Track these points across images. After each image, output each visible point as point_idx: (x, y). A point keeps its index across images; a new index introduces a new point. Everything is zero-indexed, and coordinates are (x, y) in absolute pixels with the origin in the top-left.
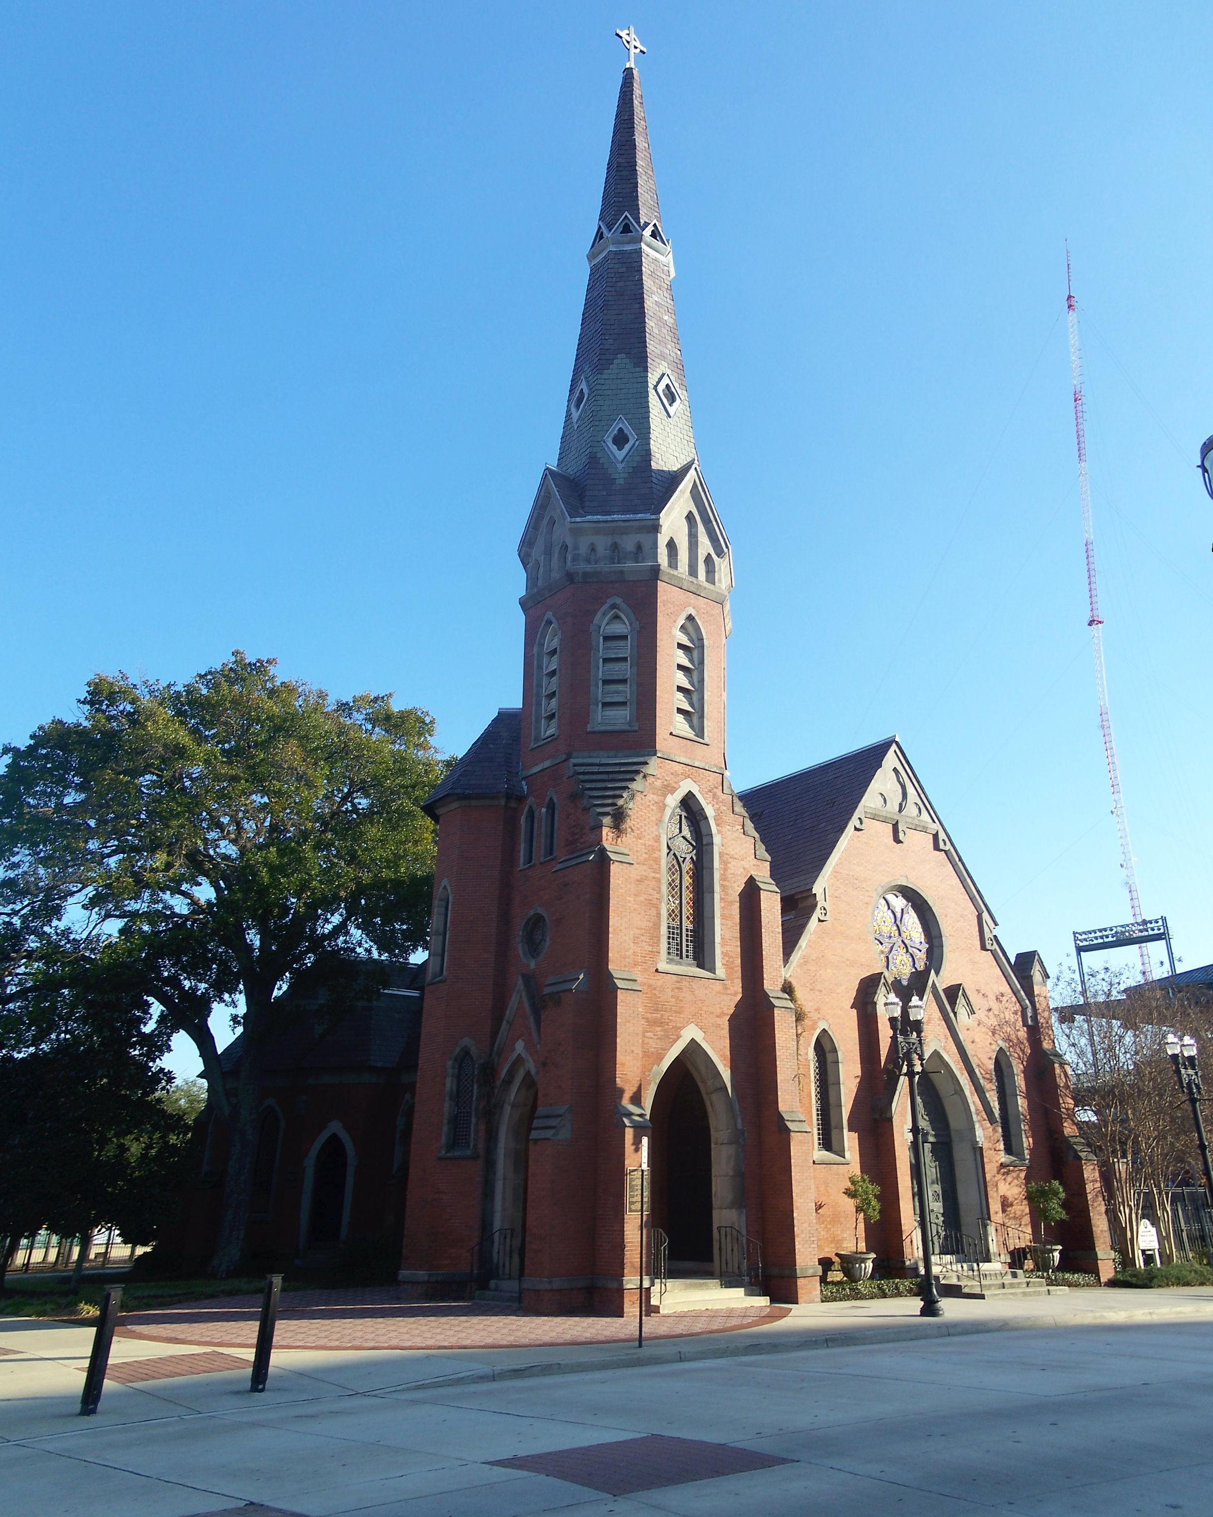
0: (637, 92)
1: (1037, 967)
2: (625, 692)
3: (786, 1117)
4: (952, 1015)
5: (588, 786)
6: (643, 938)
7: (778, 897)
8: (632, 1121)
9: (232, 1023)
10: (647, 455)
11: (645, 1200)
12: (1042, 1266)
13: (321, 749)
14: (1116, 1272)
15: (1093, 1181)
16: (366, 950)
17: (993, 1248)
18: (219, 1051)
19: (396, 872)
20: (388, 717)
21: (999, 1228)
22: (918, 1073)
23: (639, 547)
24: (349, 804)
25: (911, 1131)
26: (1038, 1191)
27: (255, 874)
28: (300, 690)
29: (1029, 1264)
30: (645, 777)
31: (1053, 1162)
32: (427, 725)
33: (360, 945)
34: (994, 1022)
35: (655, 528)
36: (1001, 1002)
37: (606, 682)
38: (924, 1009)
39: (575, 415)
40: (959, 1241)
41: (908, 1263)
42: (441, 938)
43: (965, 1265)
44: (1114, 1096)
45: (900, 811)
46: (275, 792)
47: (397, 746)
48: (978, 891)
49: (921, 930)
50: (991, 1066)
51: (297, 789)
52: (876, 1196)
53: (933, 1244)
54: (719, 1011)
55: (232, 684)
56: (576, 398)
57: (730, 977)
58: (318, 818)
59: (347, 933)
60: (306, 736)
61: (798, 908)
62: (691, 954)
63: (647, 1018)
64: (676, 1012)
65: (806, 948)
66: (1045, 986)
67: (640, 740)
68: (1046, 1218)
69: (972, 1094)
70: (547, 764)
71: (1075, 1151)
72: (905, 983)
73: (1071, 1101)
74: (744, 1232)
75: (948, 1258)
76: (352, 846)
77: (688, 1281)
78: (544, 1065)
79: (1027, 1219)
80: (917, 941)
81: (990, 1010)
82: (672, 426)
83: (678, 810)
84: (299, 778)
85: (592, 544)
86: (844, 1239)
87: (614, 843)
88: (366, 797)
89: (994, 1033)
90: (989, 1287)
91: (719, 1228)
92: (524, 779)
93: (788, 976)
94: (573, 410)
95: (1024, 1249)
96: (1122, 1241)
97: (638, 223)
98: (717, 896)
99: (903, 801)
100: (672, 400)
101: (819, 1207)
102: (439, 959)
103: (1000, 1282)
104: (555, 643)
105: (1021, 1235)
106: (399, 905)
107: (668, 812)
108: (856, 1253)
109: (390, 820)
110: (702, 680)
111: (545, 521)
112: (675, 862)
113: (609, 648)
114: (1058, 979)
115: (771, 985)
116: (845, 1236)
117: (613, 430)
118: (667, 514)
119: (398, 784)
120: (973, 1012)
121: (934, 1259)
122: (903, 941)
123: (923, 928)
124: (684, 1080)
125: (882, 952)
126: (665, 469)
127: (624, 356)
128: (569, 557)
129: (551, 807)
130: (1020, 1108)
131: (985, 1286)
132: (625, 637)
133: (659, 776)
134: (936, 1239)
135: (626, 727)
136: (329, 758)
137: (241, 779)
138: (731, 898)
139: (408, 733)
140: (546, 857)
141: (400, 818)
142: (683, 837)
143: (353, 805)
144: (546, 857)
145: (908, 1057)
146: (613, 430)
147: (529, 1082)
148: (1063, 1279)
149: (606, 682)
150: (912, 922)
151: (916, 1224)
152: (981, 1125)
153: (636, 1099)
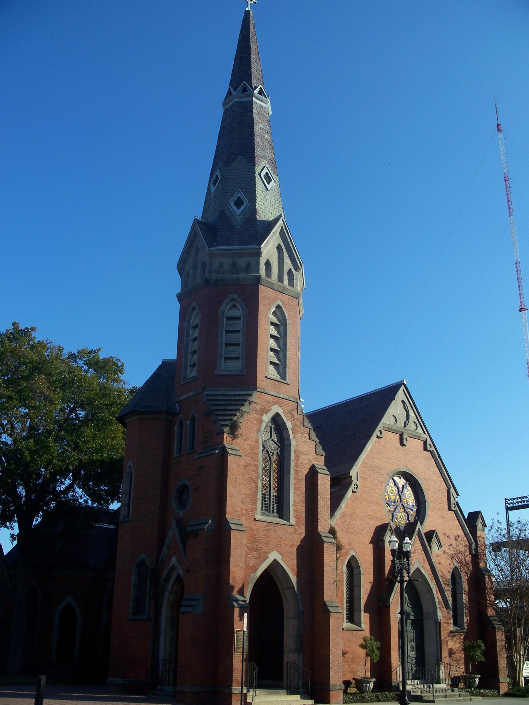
0: (252, 21)
1: (480, 520)
2: (239, 351)
3: (328, 604)
4: (428, 548)
5: (215, 408)
6: (247, 500)
7: (329, 478)
8: (238, 604)
9: (11, 539)
10: (254, 212)
11: (245, 647)
12: (469, 685)
13: (58, 381)
14: (509, 689)
15: (501, 640)
16: (85, 501)
17: (442, 676)
18: (5, 554)
19: (102, 456)
20: (97, 362)
21: (446, 666)
22: (406, 581)
23: (249, 265)
24: (74, 414)
25: (400, 613)
26: (470, 646)
27: (22, 454)
28: (48, 346)
29: (461, 685)
30: (250, 403)
31: (480, 631)
32: (119, 367)
33: (81, 498)
34: (452, 552)
35: (259, 254)
36: (458, 540)
37: (227, 345)
38: (412, 545)
39: (213, 189)
40: (423, 673)
41: (394, 684)
42: (128, 496)
43: (426, 686)
44: (517, 594)
45: (405, 426)
46: (32, 407)
47: (102, 380)
49: (413, 498)
50: (449, 576)
51: (45, 405)
52: (377, 648)
53: (409, 674)
54: (291, 543)
55: (11, 342)
56: (213, 180)
57: (298, 524)
58: (56, 422)
59: (74, 491)
60: (50, 373)
61: (341, 484)
62: (275, 510)
63: (248, 547)
64: (265, 543)
65: (344, 508)
66: (484, 531)
67: (247, 381)
68: (473, 660)
69: (437, 593)
70: (191, 394)
71: (493, 624)
72: (402, 529)
73: (493, 597)
74: (301, 666)
75: (416, 681)
76: (76, 440)
77: (269, 691)
78: (188, 571)
79: (463, 661)
80: (411, 504)
81: (451, 545)
82: (269, 196)
83: (270, 424)
84: (46, 399)
85: (221, 263)
86: (358, 671)
87: (230, 443)
88: (83, 410)
89: (452, 558)
90: (438, 697)
91: (287, 664)
92: (177, 402)
93: (333, 524)
94: (212, 186)
95: (459, 677)
96: (514, 671)
97: (251, 86)
98: (292, 477)
99: (407, 420)
100: (269, 181)
101: (344, 653)
102: (127, 508)
103: (444, 694)
104: (197, 321)
105: (458, 669)
106: (103, 475)
107: (264, 425)
108: (365, 678)
109: (98, 425)
110: (285, 345)
111: (193, 249)
112: (267, 455)
113: (229, 324)
114: (491, 528)
115: (323, 528)
116: (359, 669)
117: (235, 198)
118: (266, 246)
119: (102, 403)
120: (441, 546)
121: (409, 682)
122: (402, 505)
123: (414, 497)
124: (269, 582)
125: (390, 511)
126: (264, 219)
127: (242, 157)
128: (207, 270)
129: (193, 420)
130: (464, 601)
131: (436, 696)
132: (238, 318)
133: (258, 403)
134: (410, 671)
135: (239, 373)
136: (62, 386)
137: (13, 398)
138: (300, 478)
139: (108, 372)
140: (190, 450)
141: (103, 424)
142: (272, 440)
143: (76, 415)
144: (190, 450)
145: (401, 573)
146: (235, 198)
147: (179, 580)
148: (480, 692)
149: (227, 345)
150: (408, 493)
151: (400, 663)
152: (441, 610)
153: (241, 592)
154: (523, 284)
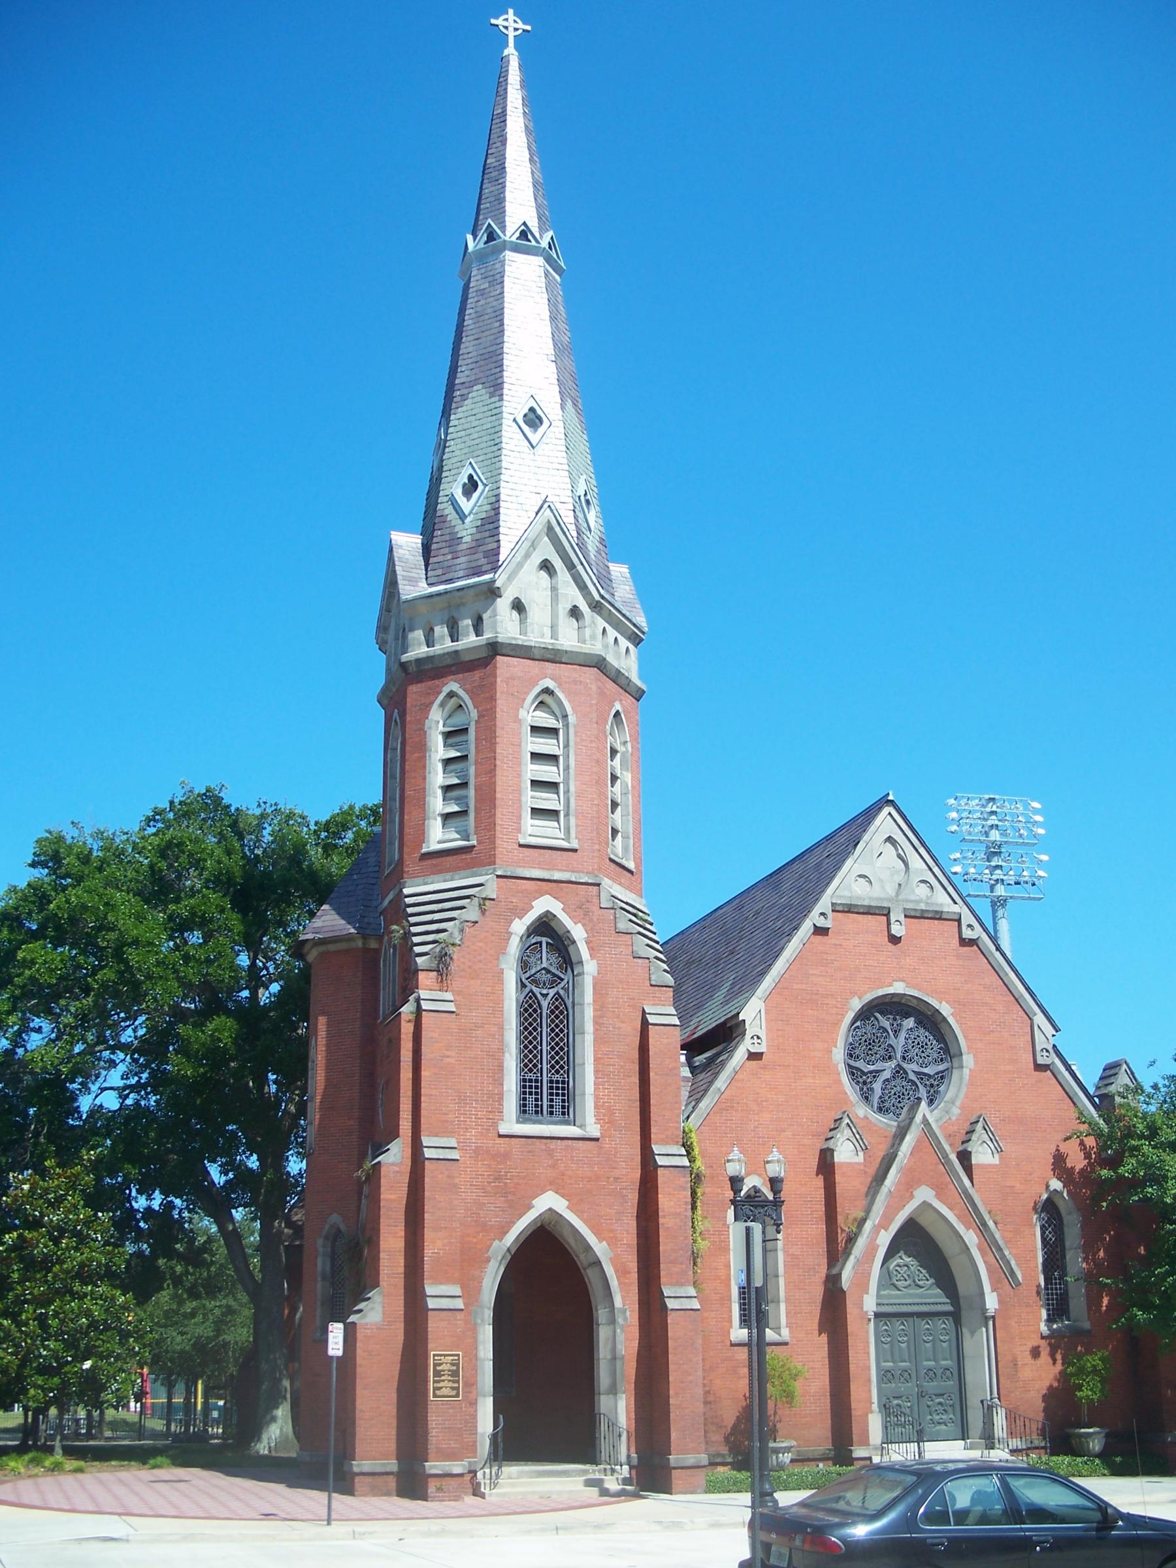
48: (1028, 989)
127: (480, 387)
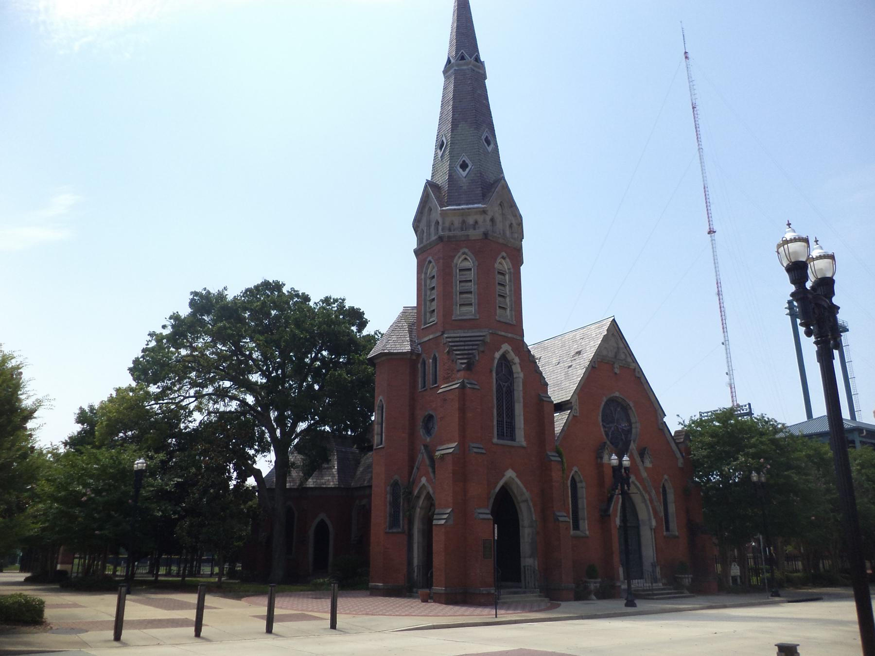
18: (52, 430)
37: (461, 293)
70: (431, 337)
111: (427, 209)
128: (440, 228)
129: (435, 359)
135: (473, 317)
147: (429, 497)
149: (461, 293)
154: (712, 207)
